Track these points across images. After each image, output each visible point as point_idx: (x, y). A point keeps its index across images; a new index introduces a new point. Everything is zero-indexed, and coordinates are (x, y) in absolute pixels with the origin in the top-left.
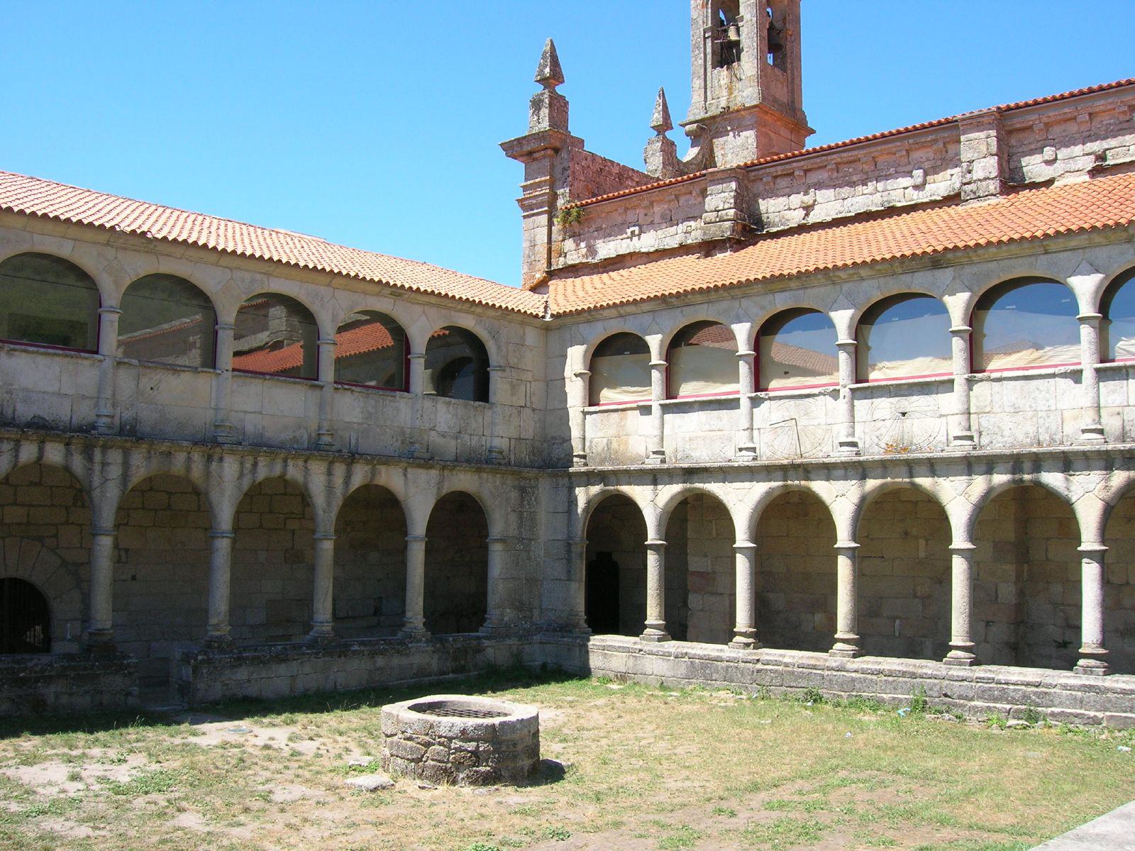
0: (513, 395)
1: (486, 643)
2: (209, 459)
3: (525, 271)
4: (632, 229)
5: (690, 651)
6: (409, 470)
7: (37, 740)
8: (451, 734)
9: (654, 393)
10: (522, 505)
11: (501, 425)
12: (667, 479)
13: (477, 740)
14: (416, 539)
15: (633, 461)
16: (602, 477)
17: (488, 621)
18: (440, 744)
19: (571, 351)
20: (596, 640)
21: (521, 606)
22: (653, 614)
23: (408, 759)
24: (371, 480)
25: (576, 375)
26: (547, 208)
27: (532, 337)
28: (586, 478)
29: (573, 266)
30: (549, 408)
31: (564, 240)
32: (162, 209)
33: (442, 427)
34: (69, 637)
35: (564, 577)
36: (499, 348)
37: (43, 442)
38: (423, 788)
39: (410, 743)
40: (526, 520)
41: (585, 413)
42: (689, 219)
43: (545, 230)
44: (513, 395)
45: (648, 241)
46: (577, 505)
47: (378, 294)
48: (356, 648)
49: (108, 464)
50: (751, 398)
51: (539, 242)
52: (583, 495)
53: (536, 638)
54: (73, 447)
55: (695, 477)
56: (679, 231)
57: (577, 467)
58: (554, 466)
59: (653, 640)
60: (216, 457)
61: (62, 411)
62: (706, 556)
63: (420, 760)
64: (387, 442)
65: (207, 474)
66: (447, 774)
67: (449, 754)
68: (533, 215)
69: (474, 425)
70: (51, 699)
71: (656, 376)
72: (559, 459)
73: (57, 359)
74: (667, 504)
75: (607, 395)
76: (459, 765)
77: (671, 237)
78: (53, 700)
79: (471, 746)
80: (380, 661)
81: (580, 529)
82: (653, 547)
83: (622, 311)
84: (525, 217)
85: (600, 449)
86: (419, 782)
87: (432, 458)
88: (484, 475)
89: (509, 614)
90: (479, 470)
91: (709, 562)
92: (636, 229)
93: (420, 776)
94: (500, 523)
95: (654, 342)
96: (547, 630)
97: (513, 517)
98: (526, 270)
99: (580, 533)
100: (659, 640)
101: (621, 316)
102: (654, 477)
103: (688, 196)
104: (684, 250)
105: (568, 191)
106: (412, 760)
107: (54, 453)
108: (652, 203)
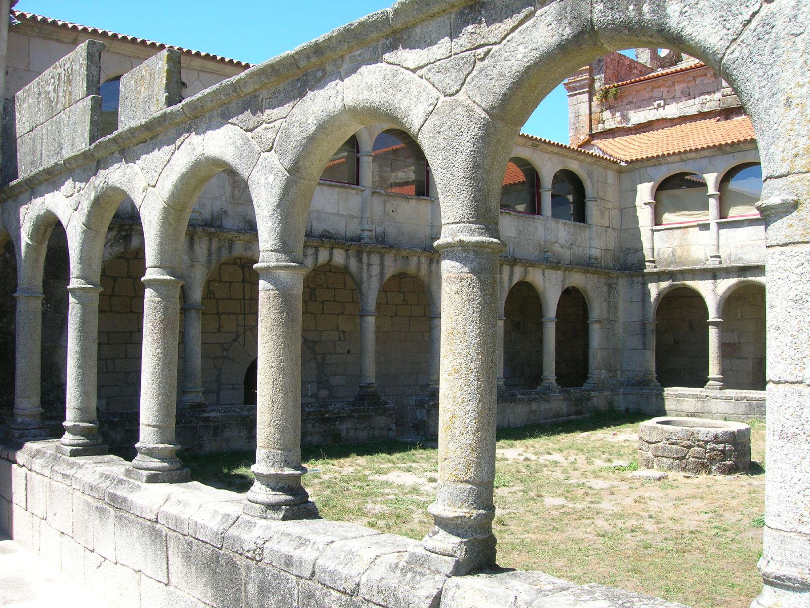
0: (602, 218)
1: (593, 394)
2: (431, 261)
3: (572, 134)
4: (658, 102)
5: (747, 395)
6: (546, 271)
7: (362, 460)
8: (706, 439)
9: (711, 215)
10: (609, 297)
11: (596, 241)
12: (724, 274)
13: (724, 442)
14: (550, 320)
15: (694, 263)
16: (671, 275)
17: (591, 379)
18: (699, 446)
19: (639, 187)
20: (668, 391)
21: (610, 368)
22: (714, 370)
23: (673, 458)
24: (524, 278)
25: (645, 204)
26: (587, 89)
27: (611, 177)
28: (657, 277)
29: (610, 130)
30: (623, 228)
31: (602, 111)
32: (130, 118)
33: (562, 241)
34: (310, 394)
35: (640, 347)
36: (593, 185)
37: (332, 249)
38: (688, 477)
39: (675, 447)
40: (612, 306)
41: (653, 231)
42: (704, 94)
43: (587, 105)
44: (602, 218)
45: (672, 111)
46: (649, 296)
47: (524, 146)
48: (520, 396)
49: (371, 265)
50: (718, 223)
51: (581, 113)
52: (654, 289)
53: (621, 391)
54: (350, 252)
55: (748, 273)
56: (697, 103)
57: (649, 268)
58: (629, 269)
59: (716, 389)
60: (435, 260)
61: (339, 227)
62: (732, 331)
63: (684, 458)
64: (529, 251)
65: (430, 272)
66: (703, 466)
67: (706, 453)
68: (577, 94)
69: (580, 239)
70: (344, 434)
71: (713, 203)
72: (633, 264)
73: (337, 189)
74: (725, 292)
75: (669, 218)
76: (712, 460)
77: (691, 107)
78: (345, 433)
79: (720, 447)
80: (534, 406)
81: (652, 312)
82: (713, 323)
83: (684, 157)
84: (569, 96)
85: (666, 256)
86: (683, 474)
87: (559, 263)
88: (588, 275)
89: (604, 374)
90: (586, 272)
91: (736, 336)
92: (662, 102)
93: (684, 469)
94: (597, 310)
95: (711, 179)
96: (627, 385)
97: (605, 305)
98: (572, 133)
99: (652, 315)
100: (721, 389)
101: (683, 161)
102: (714, 274)
103: (703, 78)
104: (702, 116)
105: (603, 76)
106: (677, 458)
107: (339, 257)
108: (674, 83)
